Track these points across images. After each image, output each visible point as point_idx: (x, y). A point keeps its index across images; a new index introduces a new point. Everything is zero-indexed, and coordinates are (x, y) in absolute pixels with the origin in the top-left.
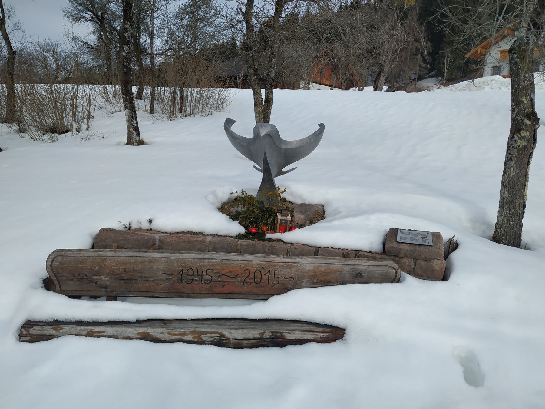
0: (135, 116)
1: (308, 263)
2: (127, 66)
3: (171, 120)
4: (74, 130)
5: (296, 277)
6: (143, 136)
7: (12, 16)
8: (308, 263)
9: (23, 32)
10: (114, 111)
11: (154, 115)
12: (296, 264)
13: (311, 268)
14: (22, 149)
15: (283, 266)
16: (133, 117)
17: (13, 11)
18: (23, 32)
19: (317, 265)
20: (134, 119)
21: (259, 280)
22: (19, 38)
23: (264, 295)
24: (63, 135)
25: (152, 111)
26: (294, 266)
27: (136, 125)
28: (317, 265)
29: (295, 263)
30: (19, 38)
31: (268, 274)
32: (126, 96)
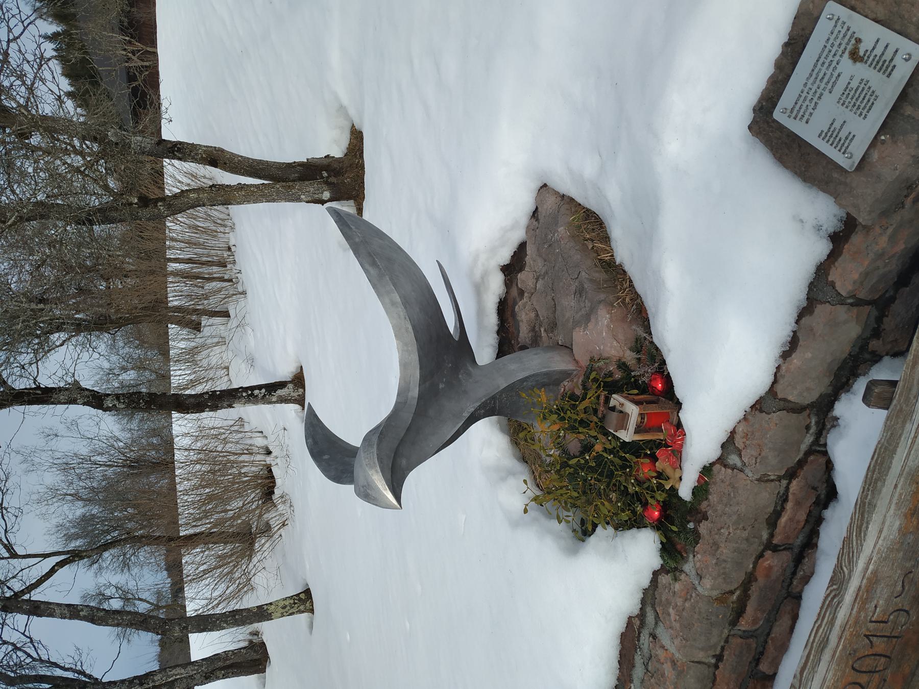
0: (245, 389)
1: (881, 532)
2: (146, 402)
3: (244, 293)
4: (269, 460)
5: (908, 565)
6: (284, 372)
7: (55, 432)
8: (881, 532)
9: (80, 417)
10: (226, 378)
11: (232, 313)
12: (871, 567)
13: (897, 523)
14: (308, 567)
15: (865, 602)
16: (249, 396)
17: (46, 430)
18: (80, 417)
19: (893, 507)
20: (252, 394)
21: (883, 660)
22: (92, 424)
23: (831, 494)
24: (278, 482)
25: (226, 314)
26: (875, 573)
27: (263, 391)
28: (893, 507)
29: (867, 569)
30: (92, 424)
31: (874, 639)
32: (208, 406)
